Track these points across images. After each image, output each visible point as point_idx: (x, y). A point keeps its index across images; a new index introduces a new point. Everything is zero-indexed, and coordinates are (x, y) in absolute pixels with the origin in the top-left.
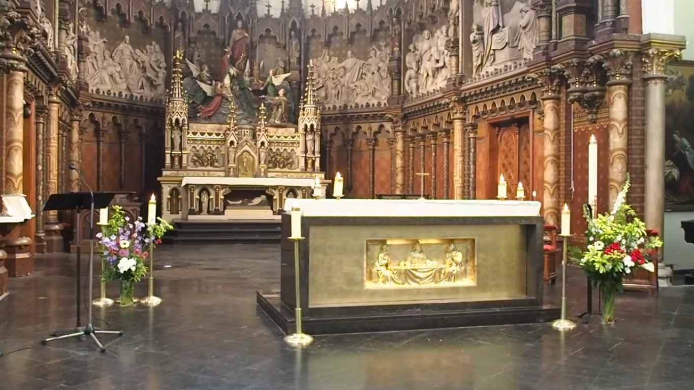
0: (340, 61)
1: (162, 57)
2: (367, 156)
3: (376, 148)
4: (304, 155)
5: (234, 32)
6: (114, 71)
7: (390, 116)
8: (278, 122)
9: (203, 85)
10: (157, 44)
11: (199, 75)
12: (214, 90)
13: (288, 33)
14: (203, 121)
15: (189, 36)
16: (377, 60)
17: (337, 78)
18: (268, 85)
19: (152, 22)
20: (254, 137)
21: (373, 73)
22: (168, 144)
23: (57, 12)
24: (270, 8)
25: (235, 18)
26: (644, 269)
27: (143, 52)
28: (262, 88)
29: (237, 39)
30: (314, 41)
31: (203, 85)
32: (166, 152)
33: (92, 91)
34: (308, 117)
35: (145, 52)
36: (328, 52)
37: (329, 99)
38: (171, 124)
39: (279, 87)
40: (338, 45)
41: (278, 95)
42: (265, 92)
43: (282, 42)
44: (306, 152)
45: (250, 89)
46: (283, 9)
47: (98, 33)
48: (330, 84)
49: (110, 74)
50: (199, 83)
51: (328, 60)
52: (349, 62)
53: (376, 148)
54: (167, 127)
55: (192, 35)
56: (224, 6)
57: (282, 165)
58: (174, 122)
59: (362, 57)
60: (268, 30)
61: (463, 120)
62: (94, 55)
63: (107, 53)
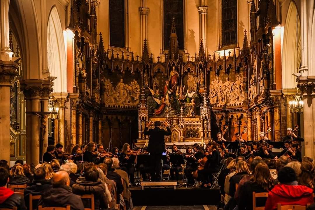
0: (223, 83)
3: (241, 126)
4: (203, 131)
5: (171, 72)
6: (116, 96)
7: (245, 110)
8: (191, 115)
9: (156, 100)
10: (136, 80)
11: (155, 95)
13: (198, 69)
14: (156, 116)
16: (240, 82)
17: (222, 91)
18: (186, 97)
21: (238, 89)
22: (139, 128)
23: (92, 83)
25: (171, 65)
27: (129, 86)
29: (173, 75)
30: (211, 72)
31: (156, 100)
32: (139, 132)
33: (107, 106)
34: (204, 112)
35: (130, 85)
36: (218, 78)
37: (219, 101)
38: (140, 119)
39: (191, 99)
40: (222, 75)
41: (191, 102)
42: (185, 101)
44: (204, 129)
47: (109, 80)
48: (219, 94)
49: (114, 97)
50: (154, 98)
51: (218, 82)
52: (227, 83)
53: (241, 126)
54: (139, 120)
57: (193, 136)
58: (141, 118)
59: (233, 80)
60: (189, 69)
61: (260, 114)
62: (107, 90)
63: (113, 88)
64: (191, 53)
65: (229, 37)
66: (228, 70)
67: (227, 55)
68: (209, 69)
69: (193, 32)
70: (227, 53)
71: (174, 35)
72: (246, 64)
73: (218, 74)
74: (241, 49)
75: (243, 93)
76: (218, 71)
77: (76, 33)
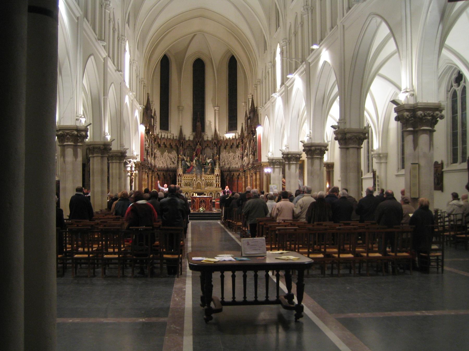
1: (176, 155)
2: (236, 182)
12: (191, 165)
19: (174, 145)
20: (201, 178)
22: (177, 181)
26: (182, 195)
30: (221, 147)
34: (217, 171)
39: (209, 163)
42: (205, 164)
48: (226, 160)
52: (231, 154)
55: (185, 147)
64: (209, 135)
65: (232, 127)
66: (232, 146)
67: (231, 137)
68: (220, 145)
69: (210, 122)
70: (230, 136)
71: (199, 124)
72: (242, 143)
73: (225, 148)
74: (240, 134)
75: (240, 160)
76: (226, 146)
77: (146, 127)
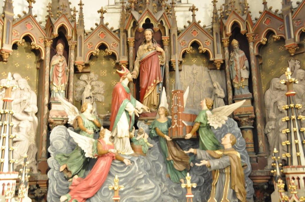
15: (75, 63)
24: (196, 13)
28: (189, 136)
39: (224, 130)
42: (195, 141)
43: (219, 58)
45: (168, 138)
46: (215, 13)
56: (126, 13)
